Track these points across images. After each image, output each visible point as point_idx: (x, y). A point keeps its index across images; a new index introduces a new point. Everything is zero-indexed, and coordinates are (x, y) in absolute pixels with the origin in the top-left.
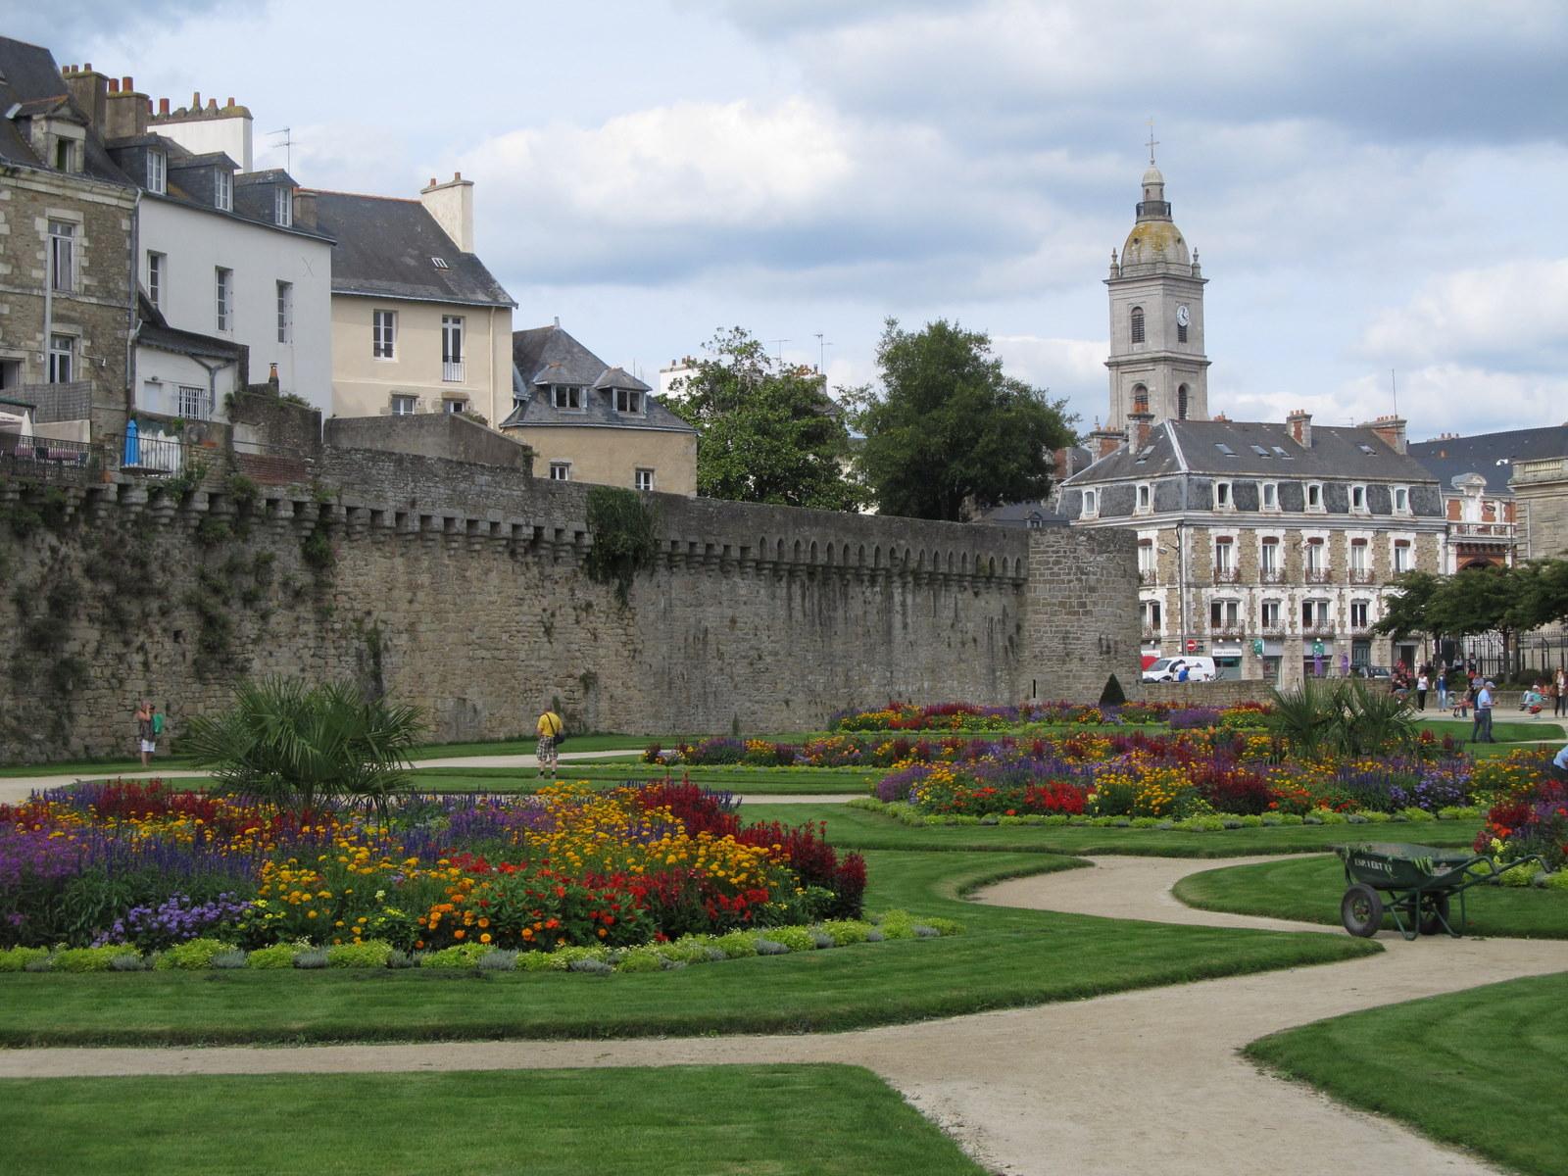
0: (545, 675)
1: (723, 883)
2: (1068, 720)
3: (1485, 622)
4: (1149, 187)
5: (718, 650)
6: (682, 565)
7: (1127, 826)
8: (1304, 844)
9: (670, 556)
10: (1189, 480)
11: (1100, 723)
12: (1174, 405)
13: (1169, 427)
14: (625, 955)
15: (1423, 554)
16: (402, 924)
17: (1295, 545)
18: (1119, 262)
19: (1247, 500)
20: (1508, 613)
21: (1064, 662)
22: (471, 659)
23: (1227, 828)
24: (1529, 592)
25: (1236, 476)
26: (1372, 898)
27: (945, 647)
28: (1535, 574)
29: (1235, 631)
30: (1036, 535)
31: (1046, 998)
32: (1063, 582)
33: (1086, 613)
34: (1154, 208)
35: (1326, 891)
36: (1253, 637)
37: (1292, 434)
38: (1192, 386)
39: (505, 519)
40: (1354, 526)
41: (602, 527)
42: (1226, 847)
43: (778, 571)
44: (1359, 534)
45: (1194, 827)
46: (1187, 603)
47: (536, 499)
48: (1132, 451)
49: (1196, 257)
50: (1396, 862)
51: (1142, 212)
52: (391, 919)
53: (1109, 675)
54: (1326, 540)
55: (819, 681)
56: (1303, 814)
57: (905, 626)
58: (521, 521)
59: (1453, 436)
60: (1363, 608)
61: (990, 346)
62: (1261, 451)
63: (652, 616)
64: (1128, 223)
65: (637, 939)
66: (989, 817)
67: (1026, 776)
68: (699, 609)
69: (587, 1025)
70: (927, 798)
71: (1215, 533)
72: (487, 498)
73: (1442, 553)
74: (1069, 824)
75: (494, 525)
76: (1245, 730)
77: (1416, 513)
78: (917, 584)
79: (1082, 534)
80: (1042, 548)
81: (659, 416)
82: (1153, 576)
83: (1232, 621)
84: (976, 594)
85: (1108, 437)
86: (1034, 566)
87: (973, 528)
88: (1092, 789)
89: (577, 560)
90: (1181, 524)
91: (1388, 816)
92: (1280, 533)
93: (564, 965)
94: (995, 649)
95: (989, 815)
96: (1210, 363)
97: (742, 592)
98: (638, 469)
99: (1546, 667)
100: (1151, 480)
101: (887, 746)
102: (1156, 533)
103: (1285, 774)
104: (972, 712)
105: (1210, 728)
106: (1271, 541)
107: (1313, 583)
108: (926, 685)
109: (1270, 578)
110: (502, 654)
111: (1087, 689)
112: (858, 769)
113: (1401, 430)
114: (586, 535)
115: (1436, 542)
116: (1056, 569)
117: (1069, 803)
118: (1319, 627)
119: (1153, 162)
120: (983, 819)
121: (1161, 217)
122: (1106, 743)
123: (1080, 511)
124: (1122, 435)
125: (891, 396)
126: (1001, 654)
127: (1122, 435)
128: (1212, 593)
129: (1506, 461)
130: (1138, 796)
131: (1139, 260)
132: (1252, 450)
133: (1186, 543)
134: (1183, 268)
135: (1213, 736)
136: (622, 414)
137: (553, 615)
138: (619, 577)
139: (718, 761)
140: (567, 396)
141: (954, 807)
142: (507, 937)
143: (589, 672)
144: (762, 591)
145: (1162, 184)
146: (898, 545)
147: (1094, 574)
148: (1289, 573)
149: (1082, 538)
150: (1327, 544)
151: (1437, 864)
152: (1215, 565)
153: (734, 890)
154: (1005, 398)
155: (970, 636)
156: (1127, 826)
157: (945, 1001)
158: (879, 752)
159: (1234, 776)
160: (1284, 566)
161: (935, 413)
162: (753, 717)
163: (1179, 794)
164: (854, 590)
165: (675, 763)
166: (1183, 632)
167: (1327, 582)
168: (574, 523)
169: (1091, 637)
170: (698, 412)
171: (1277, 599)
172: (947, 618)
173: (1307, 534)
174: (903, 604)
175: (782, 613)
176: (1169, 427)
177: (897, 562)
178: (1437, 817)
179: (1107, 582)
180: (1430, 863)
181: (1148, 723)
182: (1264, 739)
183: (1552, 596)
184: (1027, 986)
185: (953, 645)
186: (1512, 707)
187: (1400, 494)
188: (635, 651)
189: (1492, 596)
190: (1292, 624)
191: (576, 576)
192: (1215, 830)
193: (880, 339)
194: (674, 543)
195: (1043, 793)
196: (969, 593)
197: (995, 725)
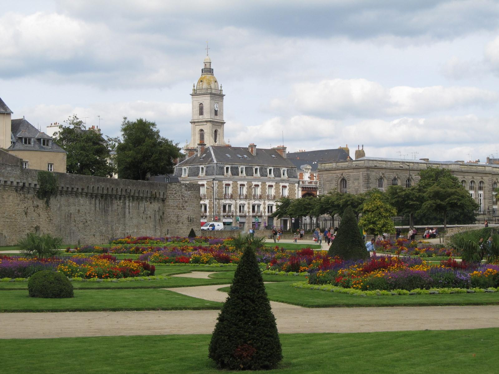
0: (25, 227)
2: (179, 242)
3: (305, 214)
5: (74, 219)
6: (65, 194)
9: (61, 191)
10: (217, 166)
12: (213, 137)
13: (211, 148)
15: (291, 190)
16: (83, 275)
17: (250, 187)
18: (195, 88)
19: (235, 172)
21: (177, 224)
22: (4, 222)
25: (232, 164)
27: (141, 219)
28: (320, 200)
29: (230, 214)
30: (169, 185)
31: (188, 286)
33: (184, 209)
34: (208, 71)
36: (236, 216)
38: (219, 130)
39: (15, 180)
40: (269, 181)
41: (42, 183)
43: (92, 196)
44: (270, 184)
46: (216, 205)
47: (24, 174)
48: (199, 156)
52: (81, 274)
53: (191, 228)
54: (260, 185)
55: (104, 229)
57: (129, 213)
58: (19, 181)
59: (303, 151)
60: (271, 207)
61: (157, 127)
62: (240, 156)
63: (55, 209)
64: (199, 74)
66: (167, 264)
67: (175, 255)
68: (69, 207)
70: (153, 259)
71: (225, 182)
72: (10, 174)
73: (297, 190)
75: (12, 182)
77: (289, 177)
79: (183, 185)
80: (171, 189)
81: (55, 147)
82: (205, 196)
83: (230, 211)
84: (151, 203)
85: (191, 151)
87: (151, 183)
88: (191, 258)
89: (35, 193)
90: (214, 180)
92: (245, 183)
94: (156, 220)
96: (225, 123)
97: (81, 202)
98: (48, 163)
101: (133, 248)
102: (206, 182)
104: (151, 239)
105: (219, 245)
106: (242, 185)
107: (255, 199)
108: (135, 230)
109: (242, 197)
110: (13, 220)
111: (184, 232)
112: (126, 254)
114: (38, 185)
116: (175, 196)
117: (185, 261)
118: (257, 213)
119: (208, 55)
121: (210, 74)
122: (192, 248)
123: (182, 174)
124: (195, 150)
125: (125, 140)
126: (158, 221)
127: (195, 150)
128: (224, 202)
129: (316, 163)
131: (202, 88)
132: (237, 156)
136: (44, 146)
137: (27, 209)
138: (46, 198)
139: (86, 252)
140: (27, 141)
142: (100, 276)
143: (37, 226)
144: (87, 202)
145: (210, 63)
146: (128, 188)
147: (187, 197)
148: (248, 196)
149: (183, 186)
150: (260, 186)
152: (224, 193)
153: (134, 271)
154: (161, 142)
155: (149, 216)
158: (131, 250)
160: (246, 193)
161: (139, 147)
162: (84, 240)
163: (210, 259)
164: (115, 201)
165: (74, 252)
166: (214, 214)
168: (34, 182)
169: (186, 216)
170: (62, 143)
171: (244, 204)
173: (254, 183)
174: (129, 206)
175: (93, 208)
176: (211, 148)
177: (128, 193)
179: (191, 200)
184: (185, 284)
187: (284, 171)
188: (50, 219)
189: (307, 206)
190: (249, 212)
191: (34, 197)
192: (218, 267)
193: (122, 123)
194: (62, 187)
195: (179, 259)
196: (149, 203)
197: (158, 243)
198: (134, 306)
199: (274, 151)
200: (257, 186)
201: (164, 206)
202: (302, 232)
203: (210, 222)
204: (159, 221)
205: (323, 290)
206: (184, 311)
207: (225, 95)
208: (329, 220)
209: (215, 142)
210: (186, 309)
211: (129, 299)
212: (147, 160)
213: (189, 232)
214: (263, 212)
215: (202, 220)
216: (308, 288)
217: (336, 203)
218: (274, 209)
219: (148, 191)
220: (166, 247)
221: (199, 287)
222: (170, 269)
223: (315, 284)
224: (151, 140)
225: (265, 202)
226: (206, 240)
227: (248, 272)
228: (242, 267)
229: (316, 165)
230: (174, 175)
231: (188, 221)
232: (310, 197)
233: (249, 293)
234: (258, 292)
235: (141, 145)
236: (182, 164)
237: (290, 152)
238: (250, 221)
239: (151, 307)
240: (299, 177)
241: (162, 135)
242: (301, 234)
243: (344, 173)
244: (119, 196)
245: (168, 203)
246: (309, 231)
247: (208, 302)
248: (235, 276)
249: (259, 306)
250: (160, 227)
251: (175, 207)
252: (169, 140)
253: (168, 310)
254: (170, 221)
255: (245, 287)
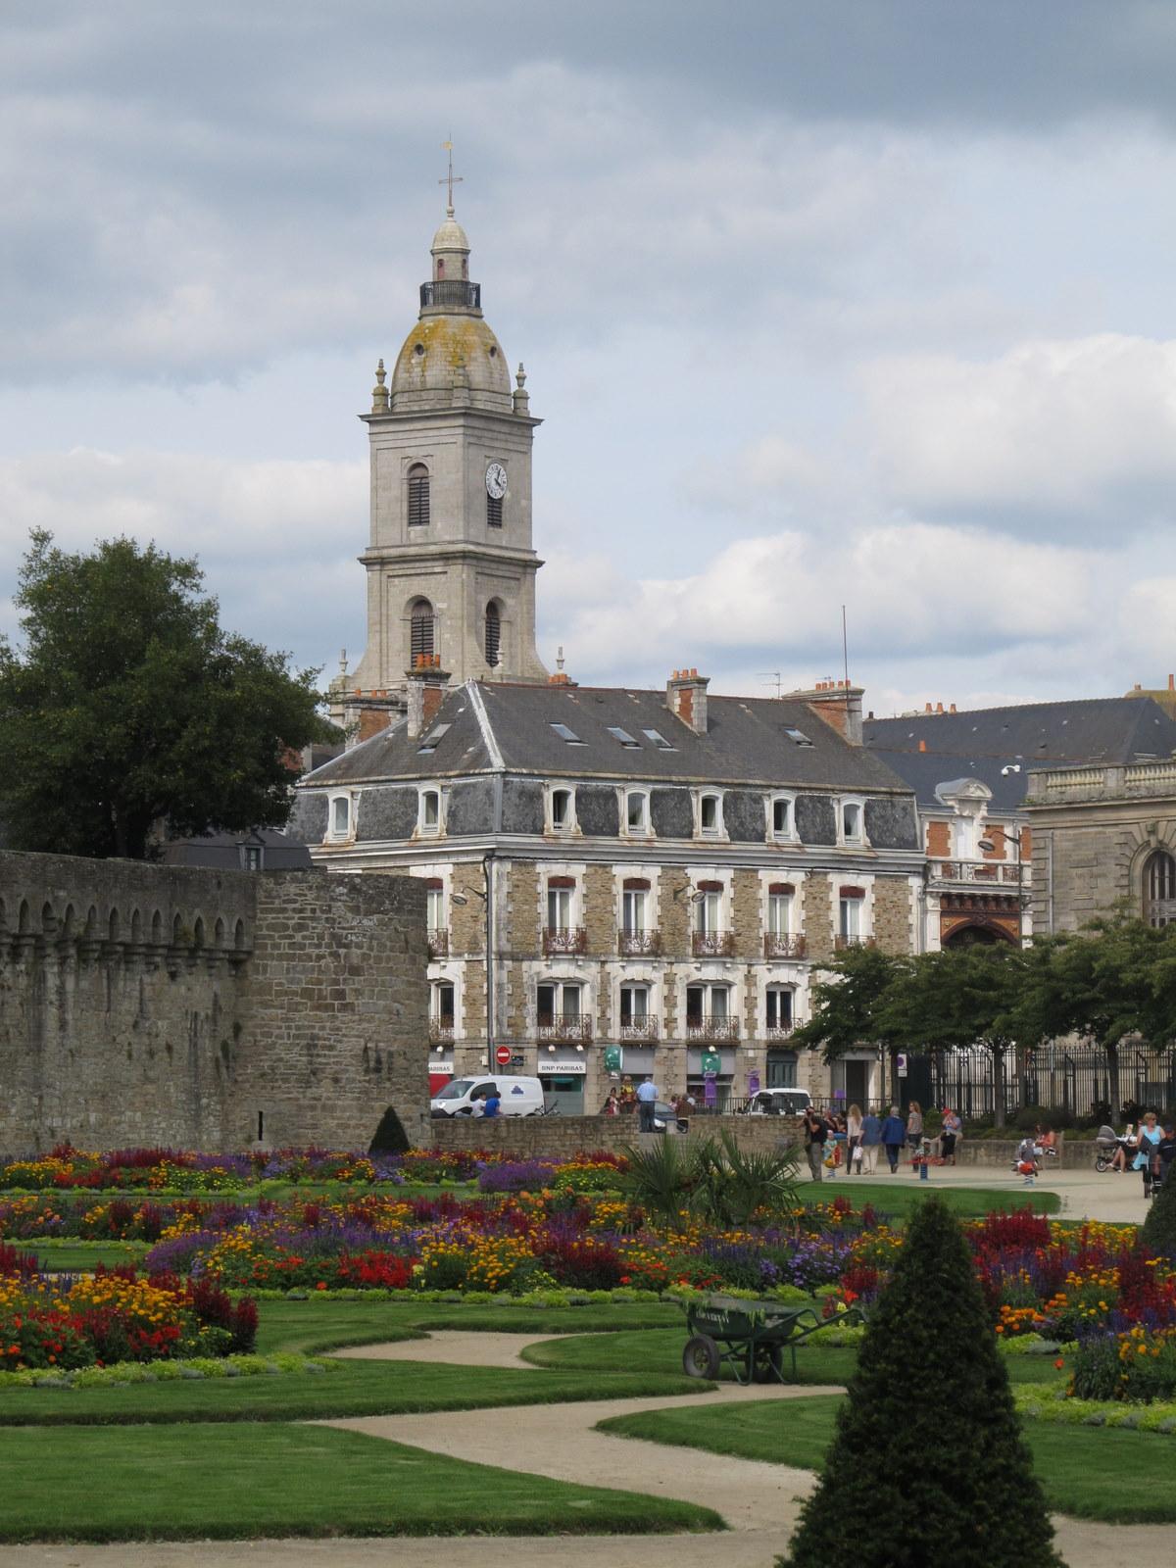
1: (143, 1322)
2: (321, 1176)
3: (966, 1031)
4: (441, 256)
7: (458, 1302)
8: (660, 1321)
10: (506, 784)
11: (371, 1181)
14: (79, 1376)
17: (676, 893)
18: (388, 384)
19: (599, 816)
20: (998, 1020)
21: (308, 1085)
23: (573, 1304)
24: (1032, 988)
26: (711, 1349)
27: (123, 1058)
28: (1044, 960)
29: (575, 1032)
30: (268, 883)
31: (434, 1408)
32: (309, 958)
33: (345, 1007)
35: (673, 1352)
36: (605, 1043)
37: (676, 709)
38: (510, 601)
40: (774, 863)
42: (572, 1322)
44: (781, 877)
45: (535, 1302)
46: (500, 985)
48: (412, 731)
49: (521, 379)
50: (731, 1313)
51: (431, 299)
54: (727, 886)
56: (659, 1290)
57: (63, 1025)
59: (947, 708)
60: (786, 998)
61: (203, 583)
62: (625, 737)
65: (80, 1363)
66: (295, 1292)
67: (335, 1244)
69: (89, 1416)
71: (545, 870)
73: (916, 909)
74: (390, 1300)
76: (592, 1194)
77: (875, 844)
78: (83, 960)
82: (444, 938)
83: (571, 1016)
84: (173, 976)
86: (265, 932)
87: (172, 873)
88: (417, 1259)
90: (490, 855)
91: (757, 1294)
92: (652, 873)
93: (31, 1382)
94: (201, 1062)
95: (295, 1289)
96: (540, 564)
99: (1101, 1097)
100: (443, 782)
101: (100, 1210)
102: (450, 869)
103: (641, 1245)
104: (181, 1163)
106: (638, 885)
107: (704, 955)
108: (93, 1118)
109: (634, 947)
112: (60, 1242)
113: (854, 706)
115: (908, 890)
116: (298, 938)
118: (714, 1026)
119: (451, 213)
120: (289, 1293)
121: (463, 309)
123: (324, 829)
126: (210, 1071)
127: (394, 703)
128: (539, 969)
129: (1017, 768)
130: (471, 1267)
131: (423, 382)
133: (499, 887)
134: (499, 398)
135: (548, 1202)
141: (254, 1279)
145: (466, 252)
146: (56, 898)
147: (359, 946)
148: (666, 939)
149: (341, 890)
150: (728, 891)
151: (769, 1316)
152: (545, 924)
154: (225, 663)
155: (161, 1041)
156: (458, 1302)
157: (358, 1405)
158: (89, 1218)
159: (582, 1246)
161: (113, 689)
163: (518, 1266)
166: (490, 1032)
167: (727, 954)
169: (352, 1045)
172: (128, 1012)
173: (697, 874)
174: (61, 991)
177: (54, 925)
178: (814, 1296)
180: (762, 1316)
181: (444, 1182)
182: (617, 1207)
183: (1067, 994)
184: (417, 1398)
185: (135, 1054)
186: (1003, 1165)
187: (850, 810)
190: (670, 1022)
193: (23, 563)
196: (162, 974)
197: (217, 1183)
198: (199, 1517)
199: (796, 708)
200: (713, 887)
201: (241, 992)
202: (951, 1124)
203: (471, 1074)
204: (217, 1067)
205: (1155, 1430)
206: (459, 1539)
207: (539, 421)
208: (1085, 1065)
209: (492, 661)
210: (471, 1527)
211: (157, 1476)
212: (155, 753)
213: (376, 1125)
214: (742, 1025)
215: (438, 1066)
216: (1074, 1421)
217: (1128, 977)
218: (802, 1010)
219: (157, 913)
220: (269, 1206)
221: (494, 1411)
222: (313, 1316)
223: (1105, 1398)
224: (173, 652)
225: (755, 970)
226: (463, 1168)
227: (931, 1336)
228: (900, 1312)
229: (1019, 782)
230: (284, 833)
231: (367, 1071)
232: (993, 948)
233: (942, 1451)
234: (989, 1445)
235: (124, 679)
236: (328, 776)
237: (877, 717)
238: (676, 1071)
239: (287, 1519)
240: (927, 843)
241: (233, 623)
242: (944, 1138)
243: (1163, 825)
244: (9, 940)
245: (260, 978)
246: (989, 1119)
247: (583, 1491)
248: (862, 1362)
249: (997, 1519)
250: (223, 1103)
251: (298, 999)
252: (268, 654)
253: (377, 1535)
254: (273, 1069)
255: (921, 1420)
